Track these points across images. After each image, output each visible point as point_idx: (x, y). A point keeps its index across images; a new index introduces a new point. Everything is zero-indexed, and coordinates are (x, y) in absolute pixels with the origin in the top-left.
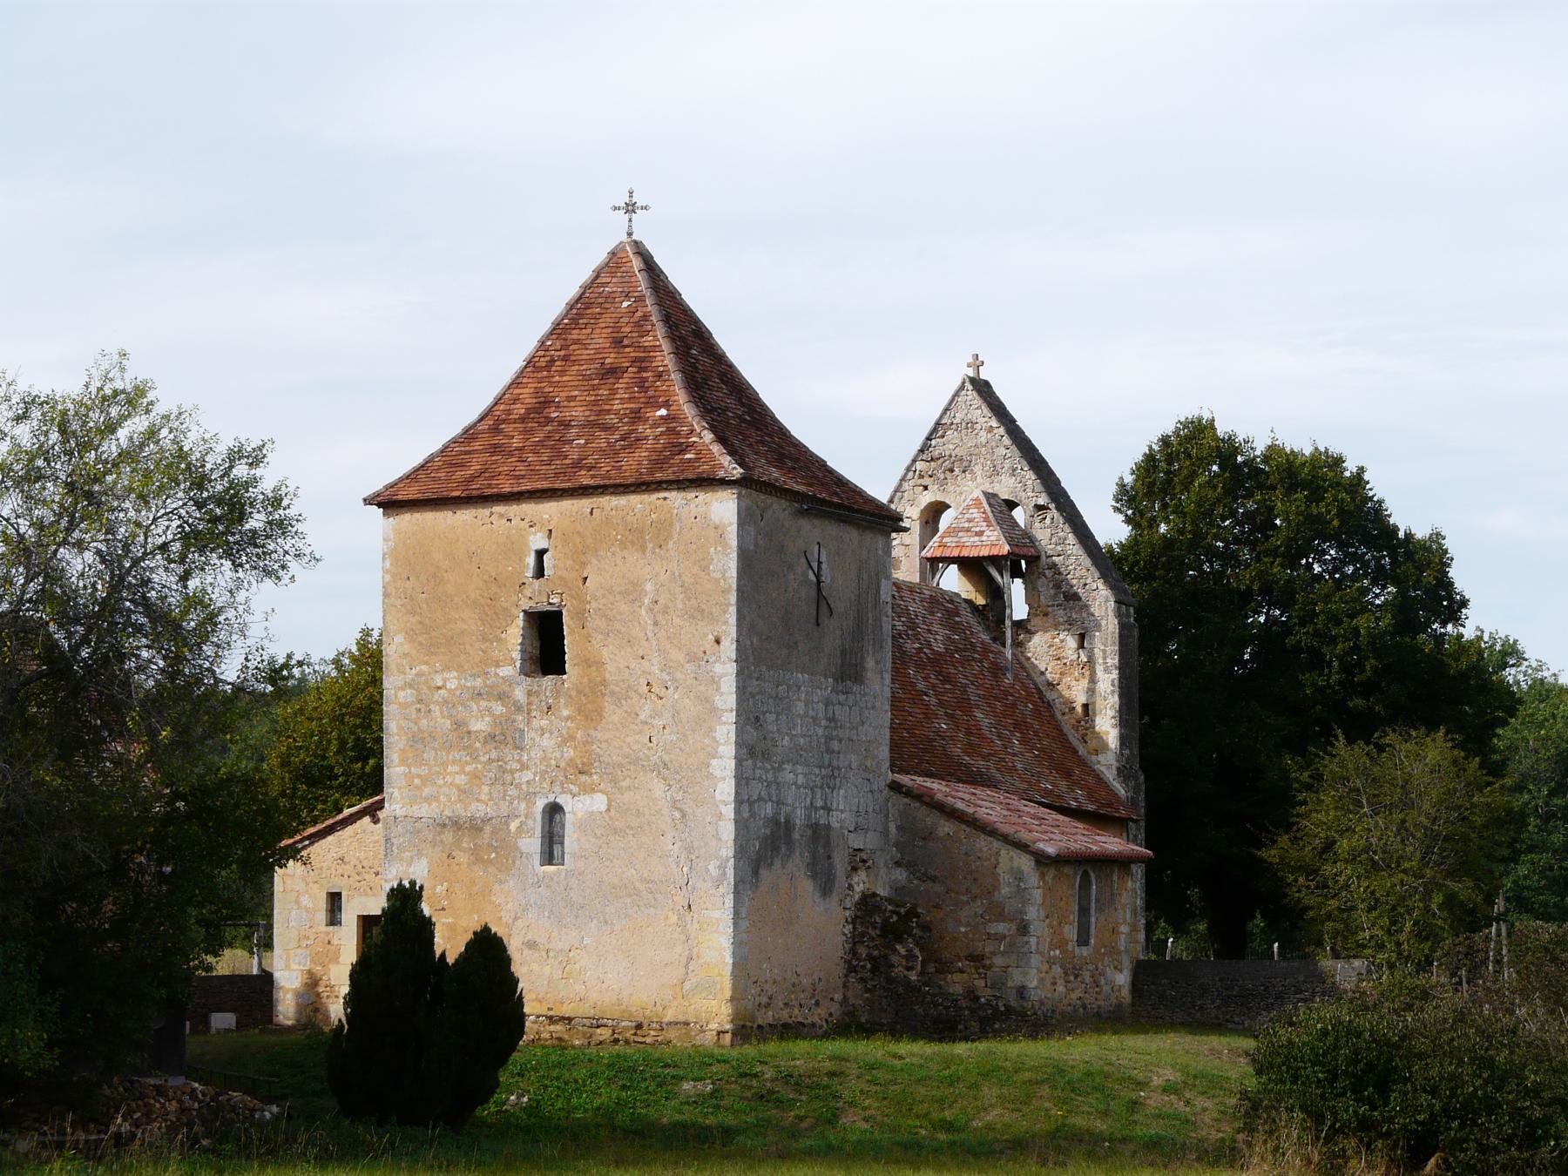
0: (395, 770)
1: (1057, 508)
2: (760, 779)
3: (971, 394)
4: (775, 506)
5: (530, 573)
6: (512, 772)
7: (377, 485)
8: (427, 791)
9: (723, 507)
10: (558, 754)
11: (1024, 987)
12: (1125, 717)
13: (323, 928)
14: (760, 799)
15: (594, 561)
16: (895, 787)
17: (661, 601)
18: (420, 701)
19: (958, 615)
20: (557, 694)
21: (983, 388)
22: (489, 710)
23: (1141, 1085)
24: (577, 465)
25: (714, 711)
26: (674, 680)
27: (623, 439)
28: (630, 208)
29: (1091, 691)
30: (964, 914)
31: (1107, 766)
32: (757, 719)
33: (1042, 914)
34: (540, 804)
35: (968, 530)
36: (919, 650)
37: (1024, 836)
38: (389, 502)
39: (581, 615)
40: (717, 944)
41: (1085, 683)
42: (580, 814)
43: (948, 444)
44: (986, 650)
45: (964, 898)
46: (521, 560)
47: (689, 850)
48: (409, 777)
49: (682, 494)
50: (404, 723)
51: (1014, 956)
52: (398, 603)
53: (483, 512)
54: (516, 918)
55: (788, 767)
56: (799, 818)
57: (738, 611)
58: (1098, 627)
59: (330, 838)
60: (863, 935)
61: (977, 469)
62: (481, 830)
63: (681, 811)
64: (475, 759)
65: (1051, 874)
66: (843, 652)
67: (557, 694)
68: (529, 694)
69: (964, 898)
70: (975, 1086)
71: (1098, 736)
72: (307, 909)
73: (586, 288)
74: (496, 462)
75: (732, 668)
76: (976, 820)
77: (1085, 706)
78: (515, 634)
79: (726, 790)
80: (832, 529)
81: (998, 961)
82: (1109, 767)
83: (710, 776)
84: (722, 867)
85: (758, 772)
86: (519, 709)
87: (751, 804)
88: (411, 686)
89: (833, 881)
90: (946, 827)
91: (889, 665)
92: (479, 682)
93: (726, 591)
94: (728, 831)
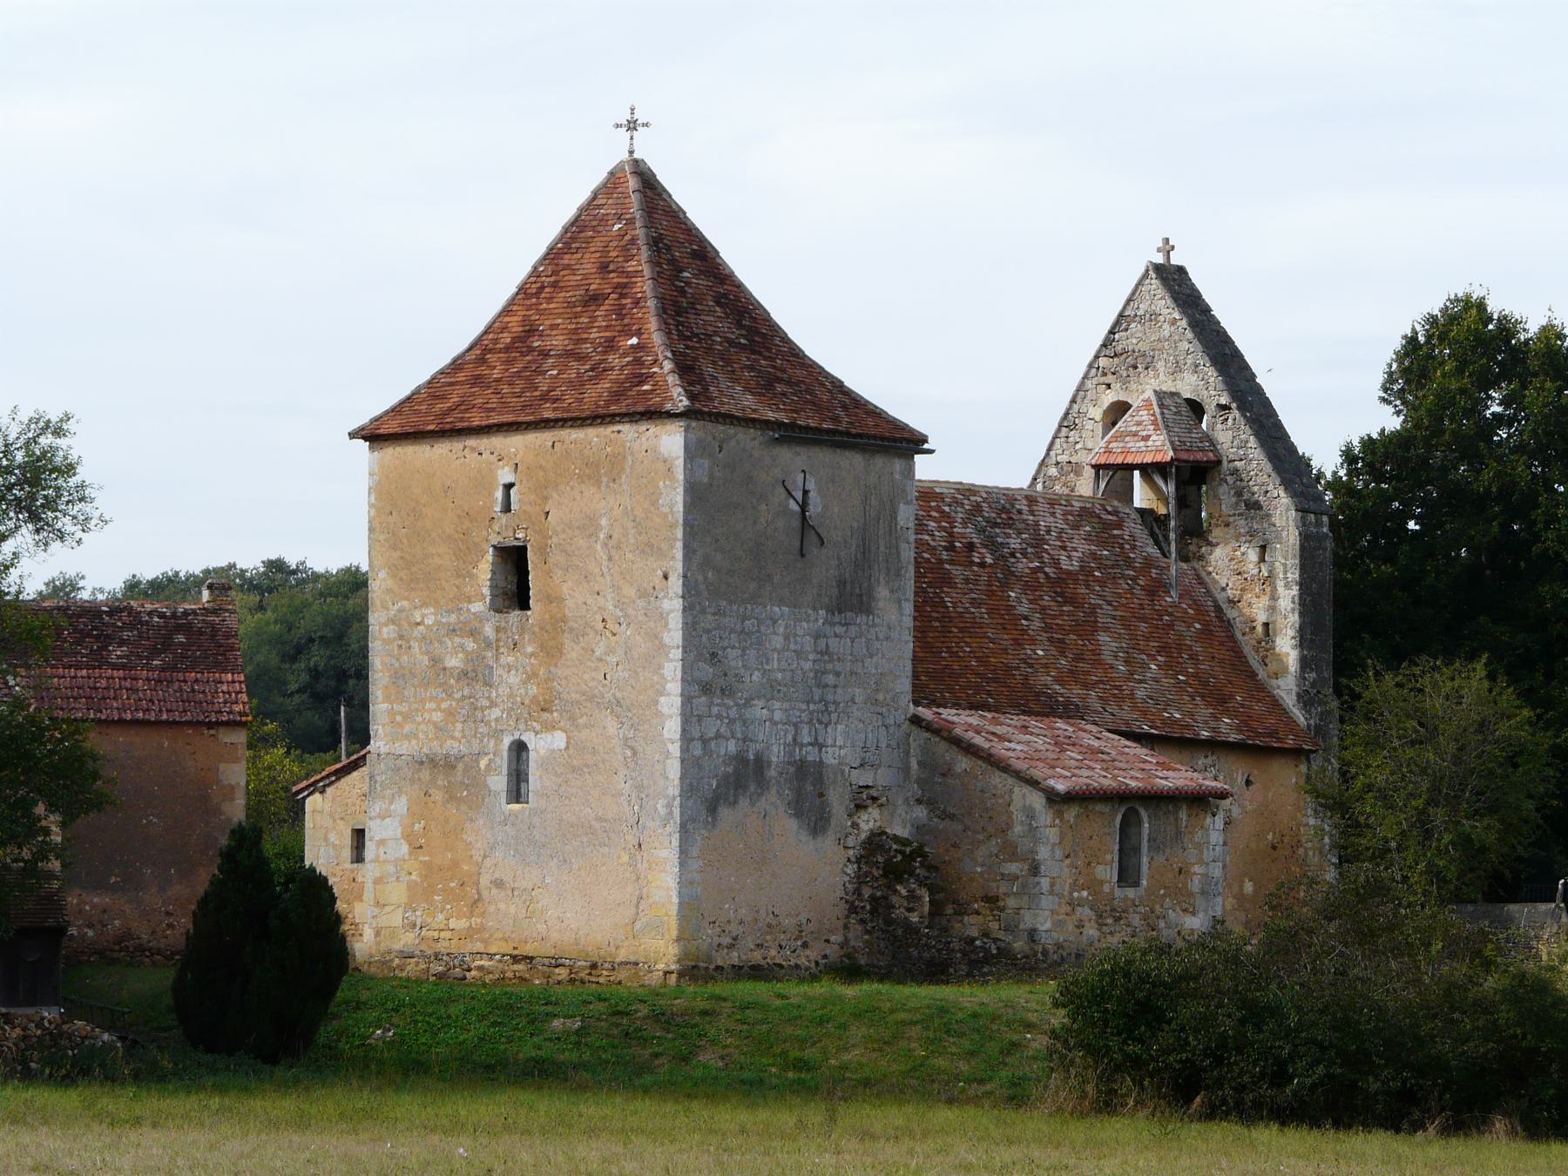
0: (380, 708)
1: (1238, 408)
2: (719, 716)
3: (1154, 283)
4: (741, 436)
5: (498, 509)
6: (482, 709)
7: (362, 419)
8: (407, 728)
9: (670, 441)
10: (522, 691)
11: (1035, 930)
12: (1305, 638)
13: (348, 866)
14: (718, 736)
15: (555, 496)
16: (916, 721)
17: (615, 536)
18: (401, 637)
19: (1119, 525)
20: (522, 630)
21: (1174, 280)
22: (462, 646)
23: (1029, 1026)
24: (545, 397)
25: (662, 647)
26: (626, 616)
27: (592, 370)
28: (632, 125)
29: (1272, 609)
30: (981, 853)
31: (1287, 689)
32: (714, 655)
33: (1059, 853)
34: (507, 741)
35: (1135, 434)
36: (1035, 570)
37: (1037, 774)
38: (373, 435)
39: (543, 550)
40: (664, 884)
41: (1265, 600)
42: (542, 752)
43: (1131, 339)
44: (1149, 563)
45: (980, 837)
46: (491, 494)
47: (639, 788)
48: (391, 713)
49: (634, 427)
50: (387, 660)
51: (1026, 898)
52: (382, 537)
53: (457, 445)
54: (485, 857)
55: (761, 703)
56: (776, 754)
57: (685, 547)
58: (1279, 538)
59: (355, 774)
60: (866, 874)
61: (1160, 365)
62: (454, 767)
63: (632, 748)
64: (450, 696)
65: (1071, 813)
66: (841, 583)
67: (522, 630)
68: (498, 630)
69: (980, 837)
70: (844, 1027)
71: (1279, 658)
72: (334, 846)
73: (582, 210)
74: (473, 394)
75: (678, 604)
76: (991, 755)
77: (1266, 625)
78: (485, 568)
79: (672, 728)
80: (823, 457)
81: (1011, 903)
82: (1289, 692)
83: (659, 714)
84: (669, 806)
85: (715, 710)
86: (489, 645)
87: (705, 741)
88: (393, 622)
89: (828, 820)
90: (963, 763)
91: (910, 594)
92: (453, 618)
93: (673, 526)
94: (674, 769)
